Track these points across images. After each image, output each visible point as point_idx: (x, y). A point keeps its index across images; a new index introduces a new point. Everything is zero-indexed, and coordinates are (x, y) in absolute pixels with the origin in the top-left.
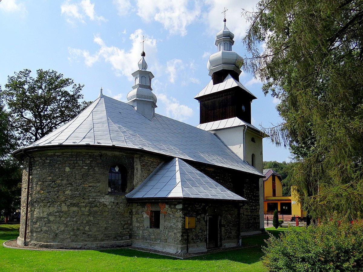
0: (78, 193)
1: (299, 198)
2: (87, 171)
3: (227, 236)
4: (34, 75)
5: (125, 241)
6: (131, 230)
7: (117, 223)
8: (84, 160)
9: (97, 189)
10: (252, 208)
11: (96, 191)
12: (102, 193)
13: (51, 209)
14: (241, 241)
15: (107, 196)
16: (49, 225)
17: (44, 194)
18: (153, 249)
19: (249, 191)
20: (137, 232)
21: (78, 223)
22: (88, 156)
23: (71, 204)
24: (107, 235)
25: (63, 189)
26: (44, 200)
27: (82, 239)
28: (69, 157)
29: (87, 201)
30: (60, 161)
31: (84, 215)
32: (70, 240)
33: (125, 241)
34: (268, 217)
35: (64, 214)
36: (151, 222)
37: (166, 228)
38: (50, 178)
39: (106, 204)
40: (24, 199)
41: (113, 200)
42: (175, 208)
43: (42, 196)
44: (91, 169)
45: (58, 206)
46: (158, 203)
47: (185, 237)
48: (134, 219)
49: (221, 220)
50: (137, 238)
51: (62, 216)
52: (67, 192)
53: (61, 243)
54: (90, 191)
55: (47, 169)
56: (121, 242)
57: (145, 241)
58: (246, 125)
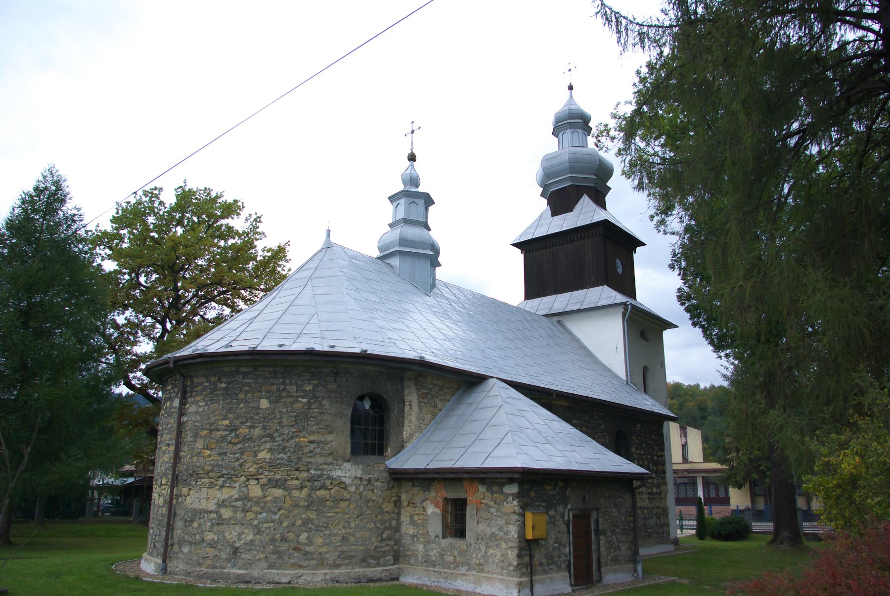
0: (285, 457)
2: (306, 407)
3: (611, 556)
4: (169, 198)
5: (385, 568)
6: (397, 542)
7: (368, 526)
8: (300, 383)
9: (326, 448)
10: (652, 489)
11: (324, 452)
12: (338, 457)
13: (226, 494)
14: (639, 568)
15: (347, 465)
16: (221, 528)
17: (212, 458)
18: (452, 587)
19: (642, 452)
20: (411, 547)
21: (285, 524)
23: (270, 480)
24: (345, 553)
25: (254, 447)
26: (212, 471)
27: (292, 561)
28: (268, 376)
29: (304, 475)
30: (249, 385)
31: (296, 506)
33: (385, 568)
34: (680, 512)
35: (253, 504)
36: (445, 526)
38: (227, 422)
39: (344, 483)
40: (163, 468)
41: (359, 474)
42: (501, 492)
43: (208, 463)
45: (240, 485)
46: (460, 480)
47: (527, 559)
48: (405, 519)
49: (597, 521)
50: (412, 561)
51: (250, 508)
52: (261, 455)
54: (311, 452)
55: (221, 402)
56: (376, 571)
57: (432, 569)
58: (628, 303)
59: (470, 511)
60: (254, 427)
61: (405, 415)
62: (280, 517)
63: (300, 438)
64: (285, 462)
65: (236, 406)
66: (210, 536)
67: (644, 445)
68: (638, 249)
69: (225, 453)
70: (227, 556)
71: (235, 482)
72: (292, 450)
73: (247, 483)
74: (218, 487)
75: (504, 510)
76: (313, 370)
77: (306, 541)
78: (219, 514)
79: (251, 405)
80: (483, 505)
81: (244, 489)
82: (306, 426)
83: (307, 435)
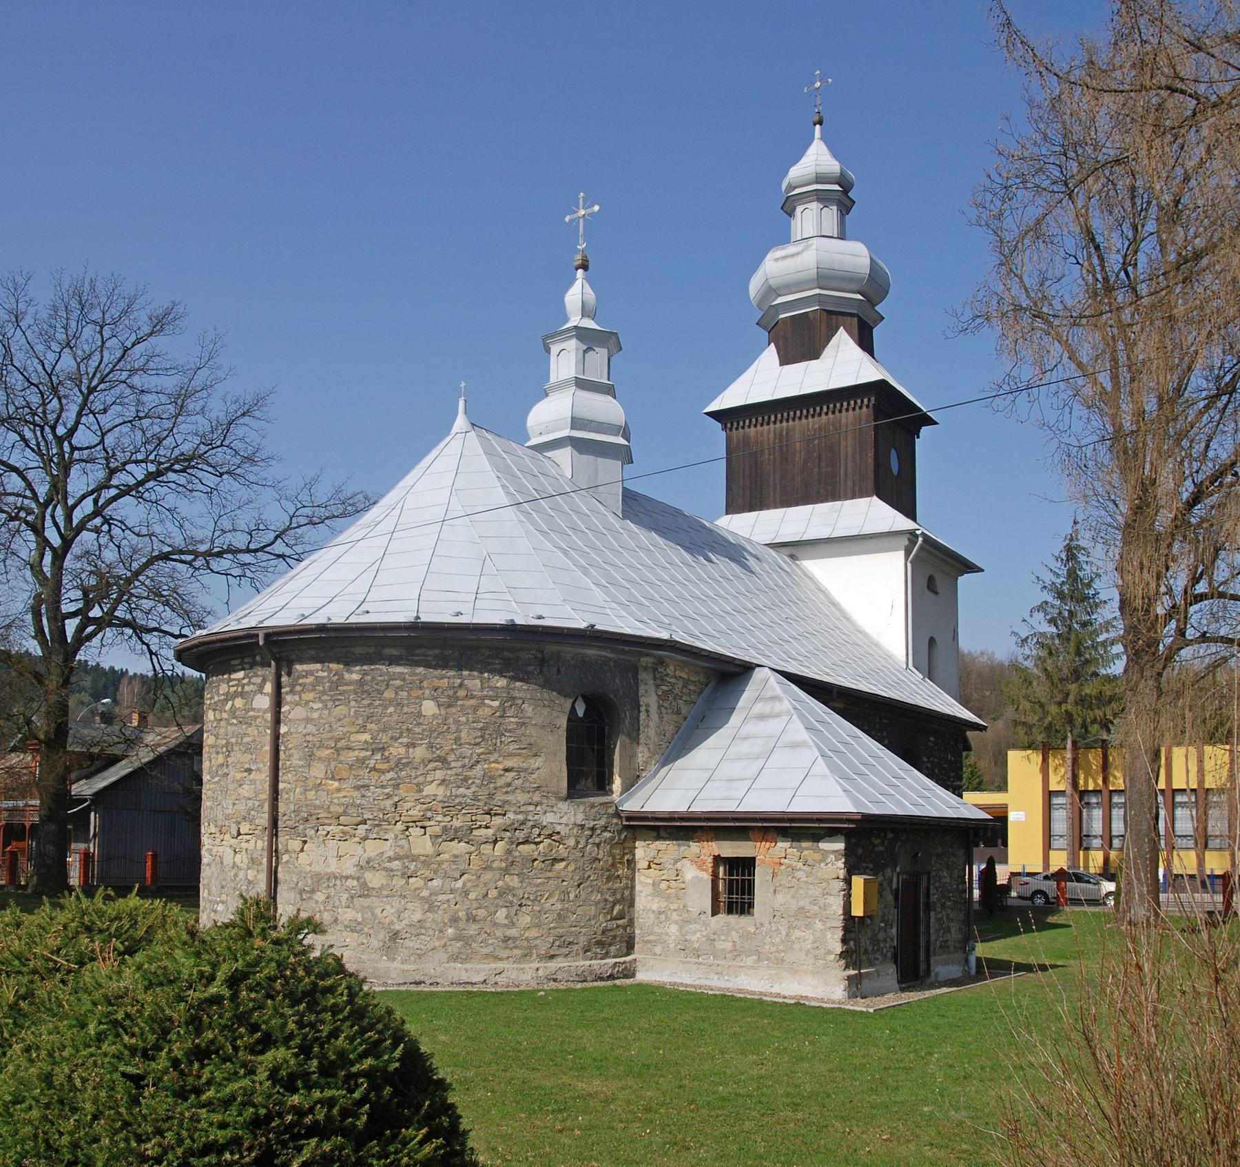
0: (469, 792)
2: (498, 714)
13: (372, 848)
20: (656, 929)
23: (445, 829)
24: (563, 939)
26: (345, 813)
27: (485, 951)
29: (498, 821)
30: (401, 677)
31: (488, 868)
32: (444, 957)
35: (419, 865)
37: (779, 914)
39: (558, 833)
41: (580, 818)
43: (336, 801)
45: (396, 837)
52: (429, 790)
53: (415, 967)
54: (509, 785)
58: (918, 532)
59: (761, 876)
60: (414, 746)
61: (641, 728)
62: (464, 884)
63: (490, 763)
64: (469, 801)
65: (380, 711)
66: (348, 915)
67: (937, 771)
68: (925, 430)
69: (367, 787)
70: (381, 944)
71: (386, 831)
72: (477, 781)
73: (407, 833)
74: (357, 839)
75: (819, 874)
76: (506, 654)
77: (506, 921)
78: (362, 880)
79: (406, 709)
80: (783, 867)
81: (403, 843)
82: (498, 744)
83: (500, 759)
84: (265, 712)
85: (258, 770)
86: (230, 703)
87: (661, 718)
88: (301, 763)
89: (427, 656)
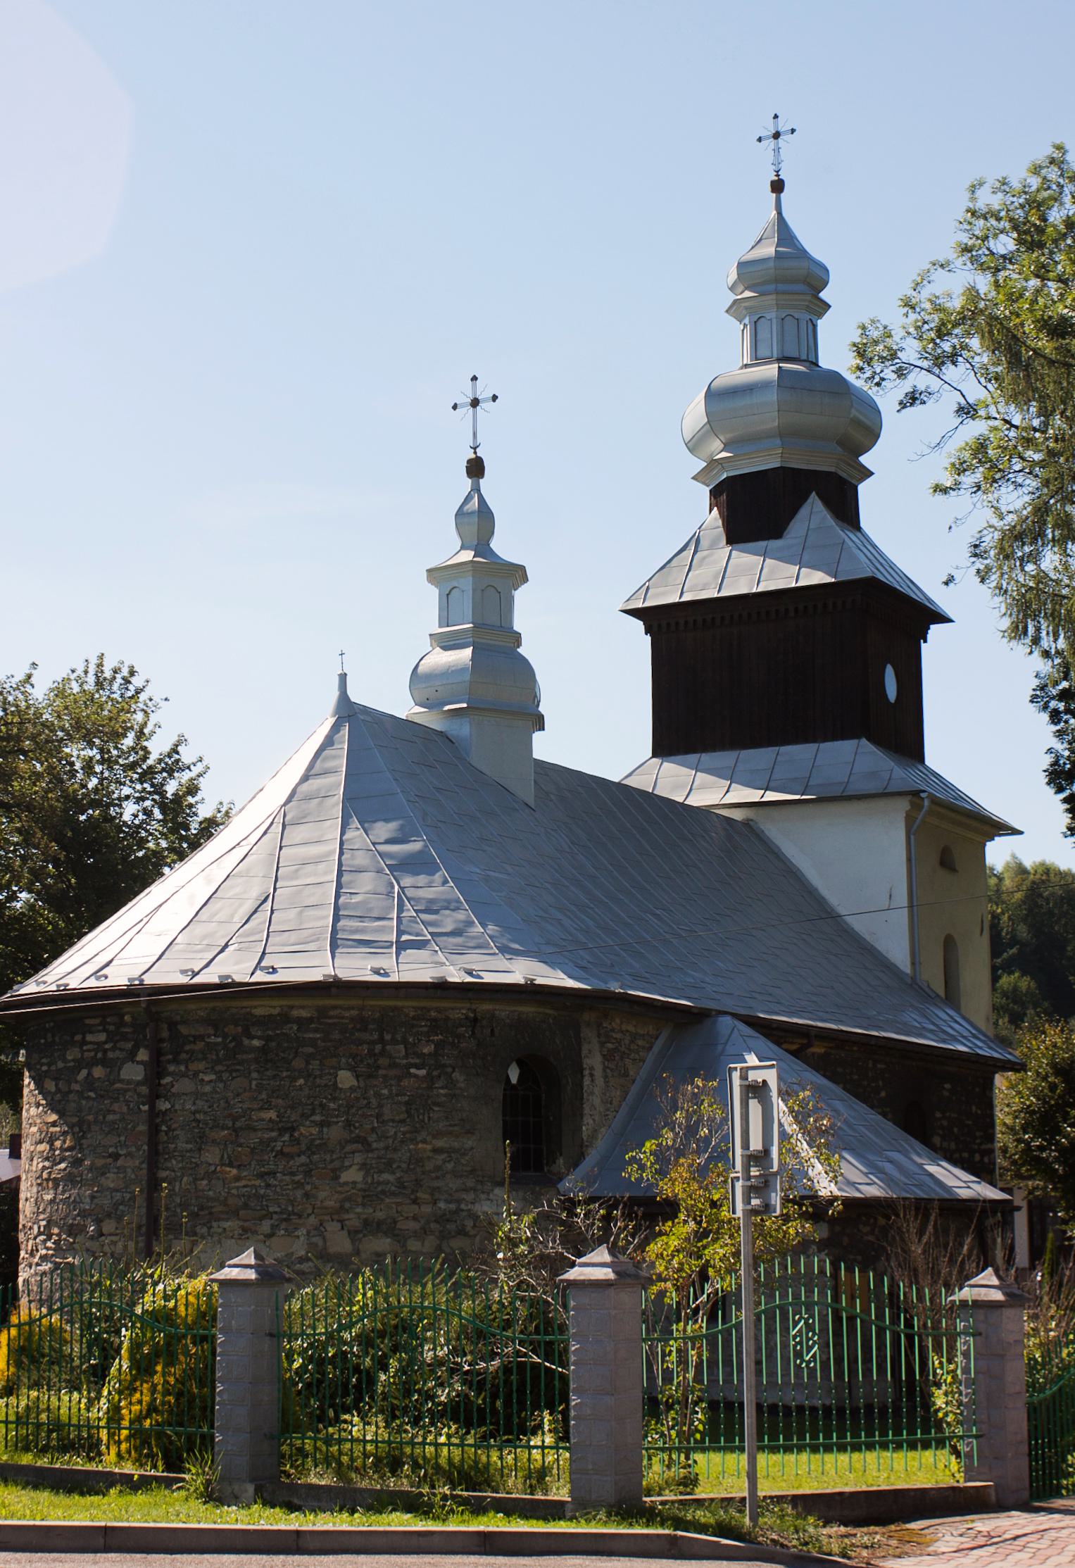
0: (391, 1178)
1: (562, 1328)
9: (463, 1161)
17: (243, 1183)
22: (426, 1026)
23: (366, 1223)
25: (332, 1161)
26: (246, 1206)
38: (272, 1114)
43: (234, 1191)
44: (439, 1076)
45: (308, 1233)
54: (438, 1168)
60: (329, 1125)
67: (956, 1130)
68: (935, 630)
84: (139, 1083)
85: (129, 1154)
86: (84, 1073)
87: (606, 1082)
88: (189, 1146)
89: (343, 1018)
